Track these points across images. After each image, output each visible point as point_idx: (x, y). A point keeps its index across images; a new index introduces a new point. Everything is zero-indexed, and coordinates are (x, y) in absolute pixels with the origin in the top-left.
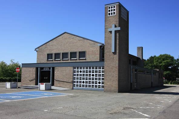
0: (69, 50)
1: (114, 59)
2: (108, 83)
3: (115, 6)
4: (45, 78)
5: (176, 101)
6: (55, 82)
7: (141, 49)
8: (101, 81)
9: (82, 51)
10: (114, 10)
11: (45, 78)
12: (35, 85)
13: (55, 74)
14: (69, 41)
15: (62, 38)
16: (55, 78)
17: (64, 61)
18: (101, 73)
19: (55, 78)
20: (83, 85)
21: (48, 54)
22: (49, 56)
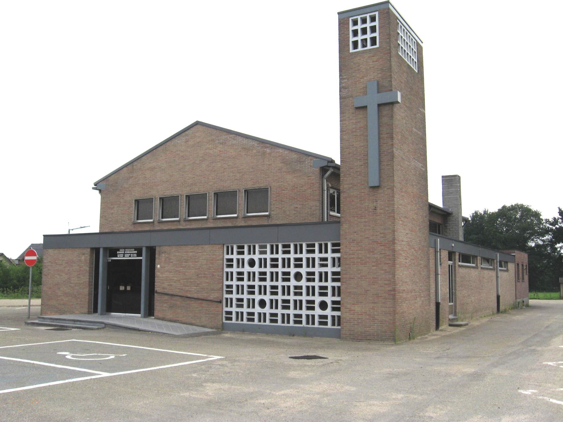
0: (208, 185)
1: (379, 211)
2: (357, 308)
3: (377, 13)
4: (129, 288)
5: (440, 330)
6: (158, 306)
7: (451, 183)
8: (328, 299)
9: (256, 186)
10: (373, 29)
11: (122, 288)
12: (89, 313)
13: (157, 274)
14: (211, 152)
15: (187, 141)
16: (158, 287)
17: (194, 226)
18: (330, 269)
19: (157, 289)
20: (260, 314)
21: (137, 202)
22: (142, 206)
